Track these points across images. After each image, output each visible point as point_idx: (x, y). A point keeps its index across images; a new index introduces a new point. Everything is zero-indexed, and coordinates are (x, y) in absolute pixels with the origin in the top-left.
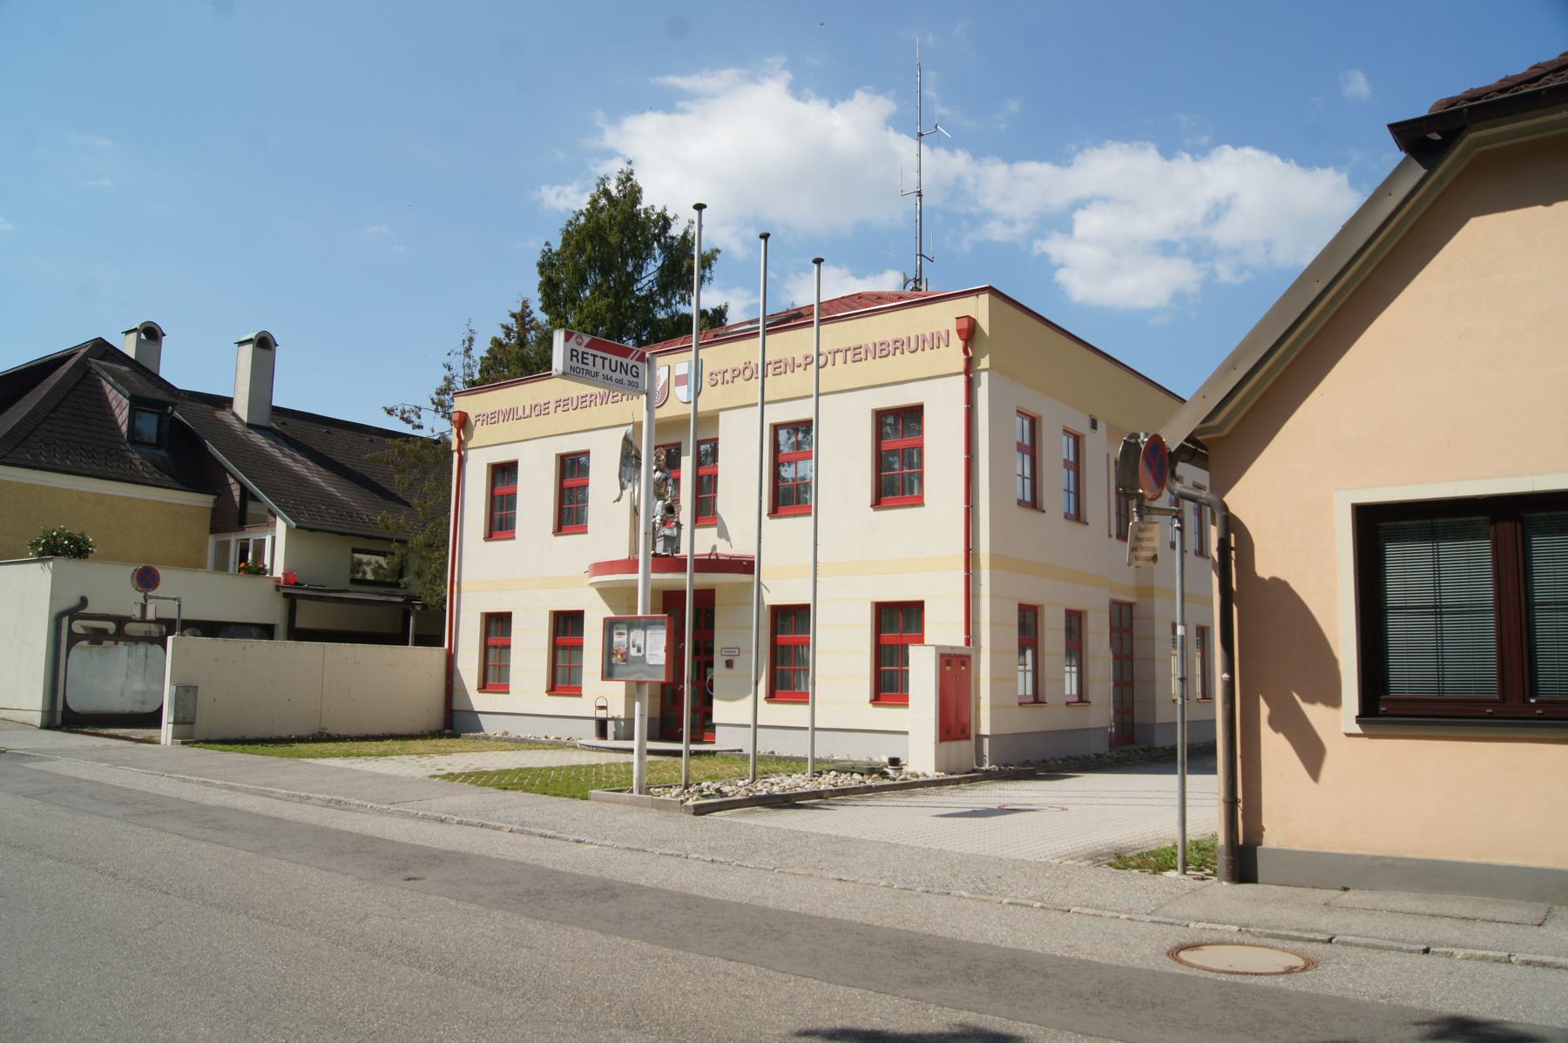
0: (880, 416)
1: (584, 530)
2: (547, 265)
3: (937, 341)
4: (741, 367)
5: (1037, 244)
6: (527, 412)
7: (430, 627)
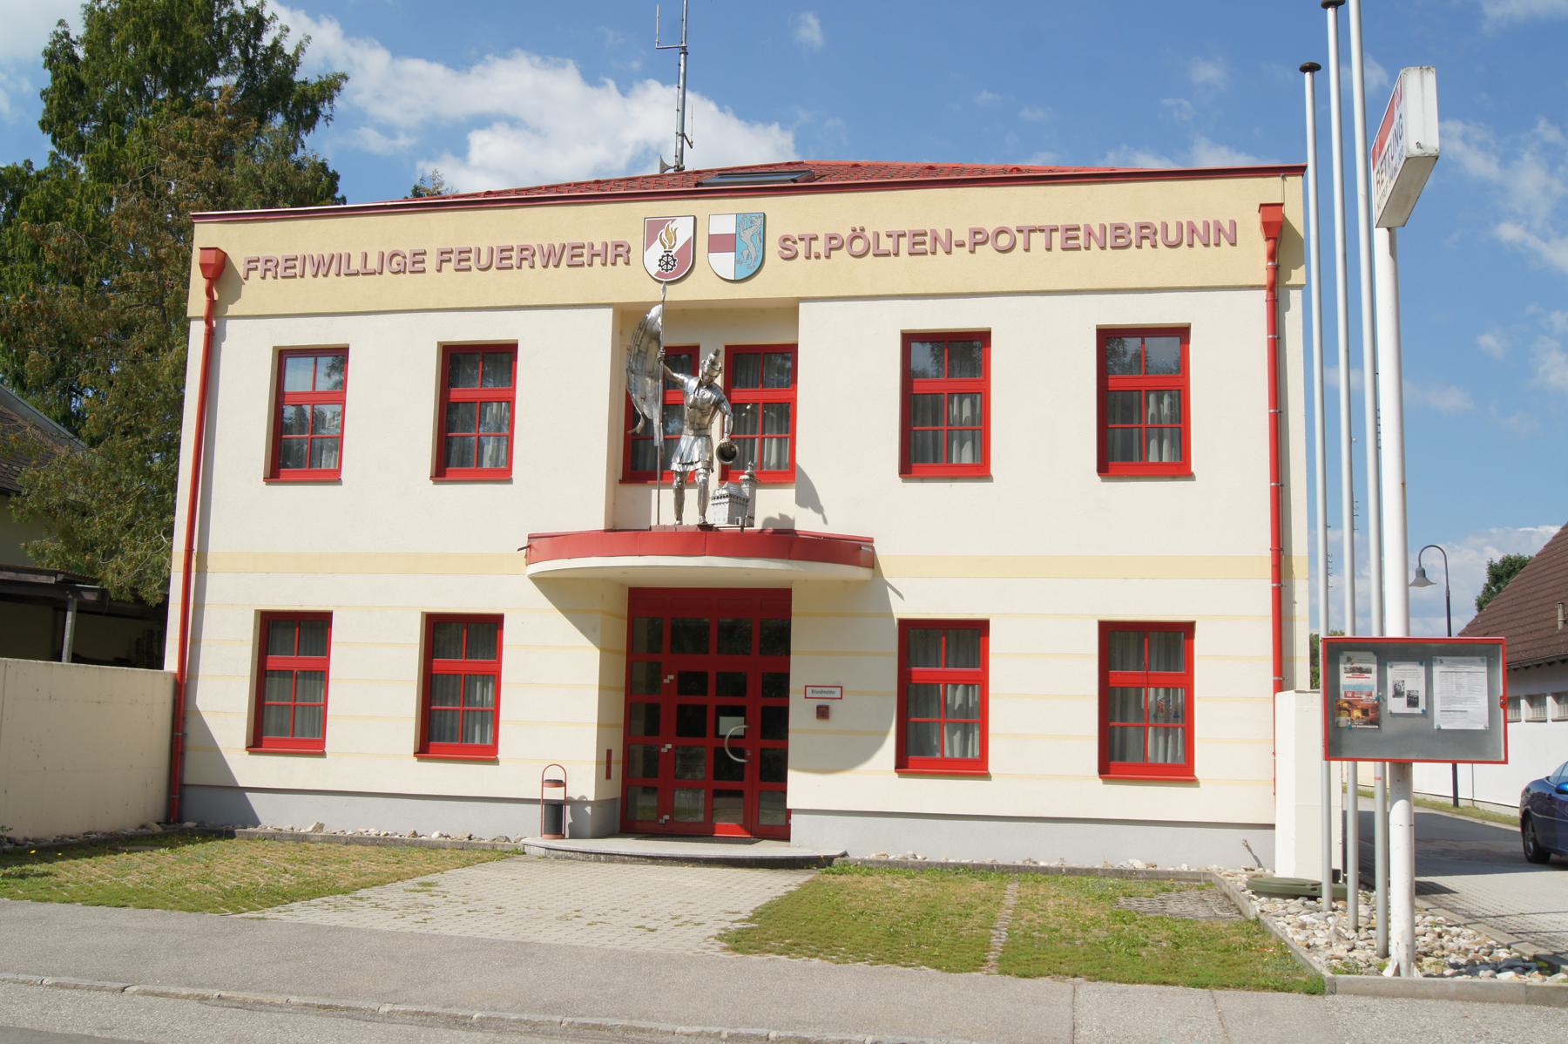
0: (910, 339)
1: (980, 470)
2: (58, 55)
3: (1220, 234)
4: (846, 234)
5: (421, 165)
6: (373, 264)
7: (130, 629)
